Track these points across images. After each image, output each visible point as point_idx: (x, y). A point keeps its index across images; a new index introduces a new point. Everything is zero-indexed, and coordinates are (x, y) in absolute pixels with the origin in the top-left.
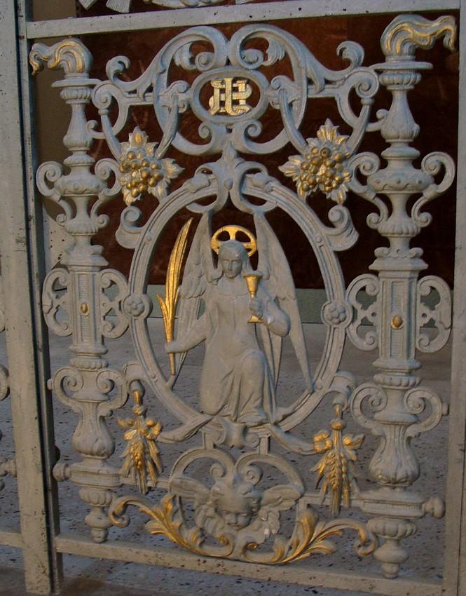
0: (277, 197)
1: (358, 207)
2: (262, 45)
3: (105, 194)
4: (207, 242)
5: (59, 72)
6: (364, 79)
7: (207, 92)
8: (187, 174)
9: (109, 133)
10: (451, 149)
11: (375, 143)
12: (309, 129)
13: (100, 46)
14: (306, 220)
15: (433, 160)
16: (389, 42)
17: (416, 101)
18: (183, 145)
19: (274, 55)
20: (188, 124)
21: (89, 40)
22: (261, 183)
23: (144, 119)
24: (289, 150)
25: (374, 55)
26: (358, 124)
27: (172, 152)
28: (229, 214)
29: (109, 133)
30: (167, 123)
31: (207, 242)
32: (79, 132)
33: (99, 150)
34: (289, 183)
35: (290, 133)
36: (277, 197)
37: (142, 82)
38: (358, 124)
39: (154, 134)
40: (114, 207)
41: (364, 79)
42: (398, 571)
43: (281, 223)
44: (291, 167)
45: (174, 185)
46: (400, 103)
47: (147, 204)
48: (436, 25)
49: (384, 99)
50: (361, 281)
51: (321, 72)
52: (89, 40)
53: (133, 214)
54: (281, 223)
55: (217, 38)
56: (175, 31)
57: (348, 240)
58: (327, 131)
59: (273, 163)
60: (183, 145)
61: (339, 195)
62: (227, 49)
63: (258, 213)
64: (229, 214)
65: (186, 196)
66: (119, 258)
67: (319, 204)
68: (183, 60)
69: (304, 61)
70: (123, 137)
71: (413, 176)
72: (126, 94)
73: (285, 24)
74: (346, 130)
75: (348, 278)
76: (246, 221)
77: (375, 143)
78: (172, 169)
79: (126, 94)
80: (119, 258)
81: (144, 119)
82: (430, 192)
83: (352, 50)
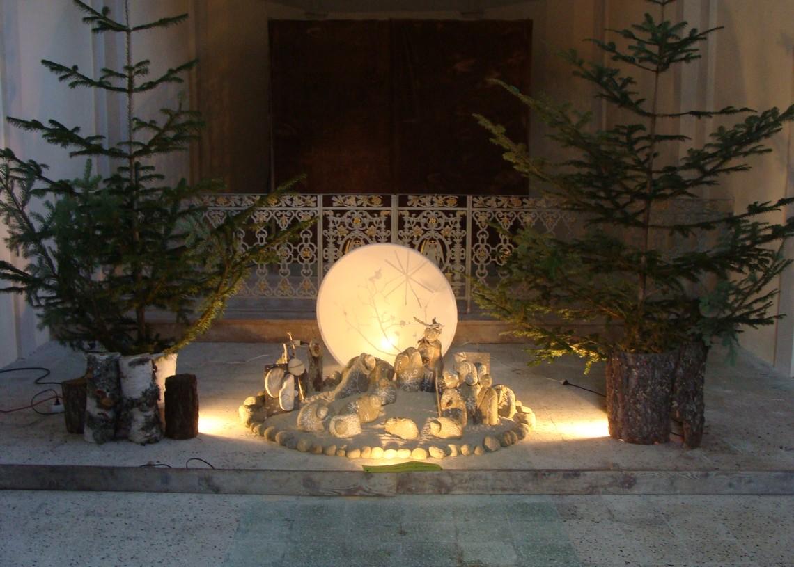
0: (440, 236)
1: (452, 238)
2: (437, 213)
3: (411, 236)
4: (428, 243)
5: (404, 216)
6: (378, 219)
7: (353, 220)
8: (425, 233)
9: (412, 226)
10: (390, 230)
11: (454, 229)
12: (445, 226)
13: (411, 212)
14: (444, 239)
15: (463, 231)
16: (381, 214)
17: (385, 222)
18: (350, 228)
19: (364, 215)
20: (426, 225)
21: (409, 211)
22: (437, 234)
23: (418, 224)
24: (366, 229)
25: (455, 216)
26: (452, 226)
27: (348, 229)
28: (432, 239)
29: (412, 226)
30: (423, 225)
31: (428, 243)
32: (407, 225)
33: (410, 228)
34: (441, 234)
35: (442, 227)
36: (440, 236)
37: (342, 218)
38: (452, 226)
39: (344, 226)
40: (412, 238)
41: (378, 219)
42: (112, 271)
43: (440, 240)
44: (442, 232)
45: (423, 234)
46: (383, 223)
47: (418, 237)
48: (389, 212)
49: (456, 222)
50: (452, 249)
51: (447, 218)
52: (409, 211)
53: (415, 239)
54: (440, 240)
55: (431, 212)
56: (423, 211)
57: (450, 243)
58: (448, 227)
59: (439, 231)
60: (350, 228)
61: (449, 236)
62: (356, 214)
63: (437, 239)
64: (432, 239)
65: (425, 236)
66: (337, 246)
67: (446, 238)
68: (425, 215)
69: (369, 216)
70: (415, 226)
71: (408, 234)
72: (340, 220)
73: (443, 211)
74: (450, 226)
75: (450, 248)
76: (359, 240)
77: (454, 229)
78: (423, 232)
79: (415, 220)
80: (337, 246)
81: (418, 224)
82: (463, 236)
83: (451, 215)
